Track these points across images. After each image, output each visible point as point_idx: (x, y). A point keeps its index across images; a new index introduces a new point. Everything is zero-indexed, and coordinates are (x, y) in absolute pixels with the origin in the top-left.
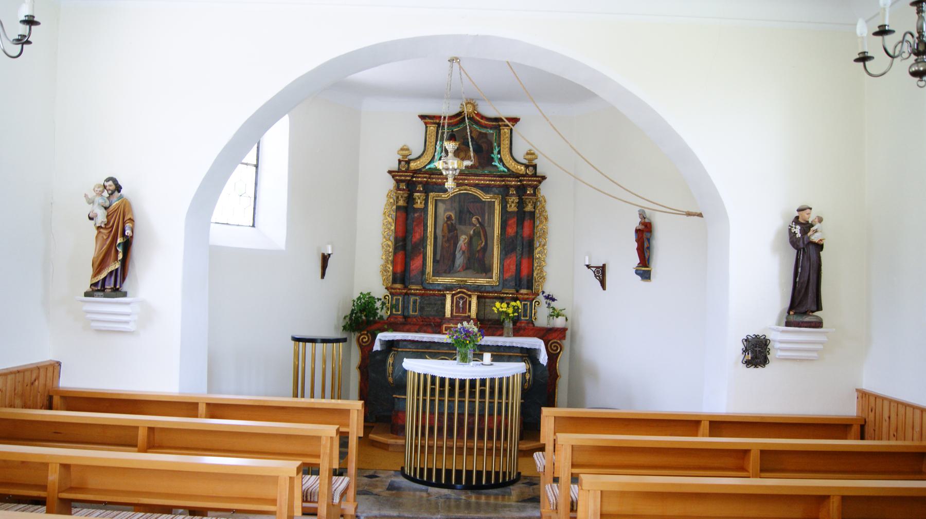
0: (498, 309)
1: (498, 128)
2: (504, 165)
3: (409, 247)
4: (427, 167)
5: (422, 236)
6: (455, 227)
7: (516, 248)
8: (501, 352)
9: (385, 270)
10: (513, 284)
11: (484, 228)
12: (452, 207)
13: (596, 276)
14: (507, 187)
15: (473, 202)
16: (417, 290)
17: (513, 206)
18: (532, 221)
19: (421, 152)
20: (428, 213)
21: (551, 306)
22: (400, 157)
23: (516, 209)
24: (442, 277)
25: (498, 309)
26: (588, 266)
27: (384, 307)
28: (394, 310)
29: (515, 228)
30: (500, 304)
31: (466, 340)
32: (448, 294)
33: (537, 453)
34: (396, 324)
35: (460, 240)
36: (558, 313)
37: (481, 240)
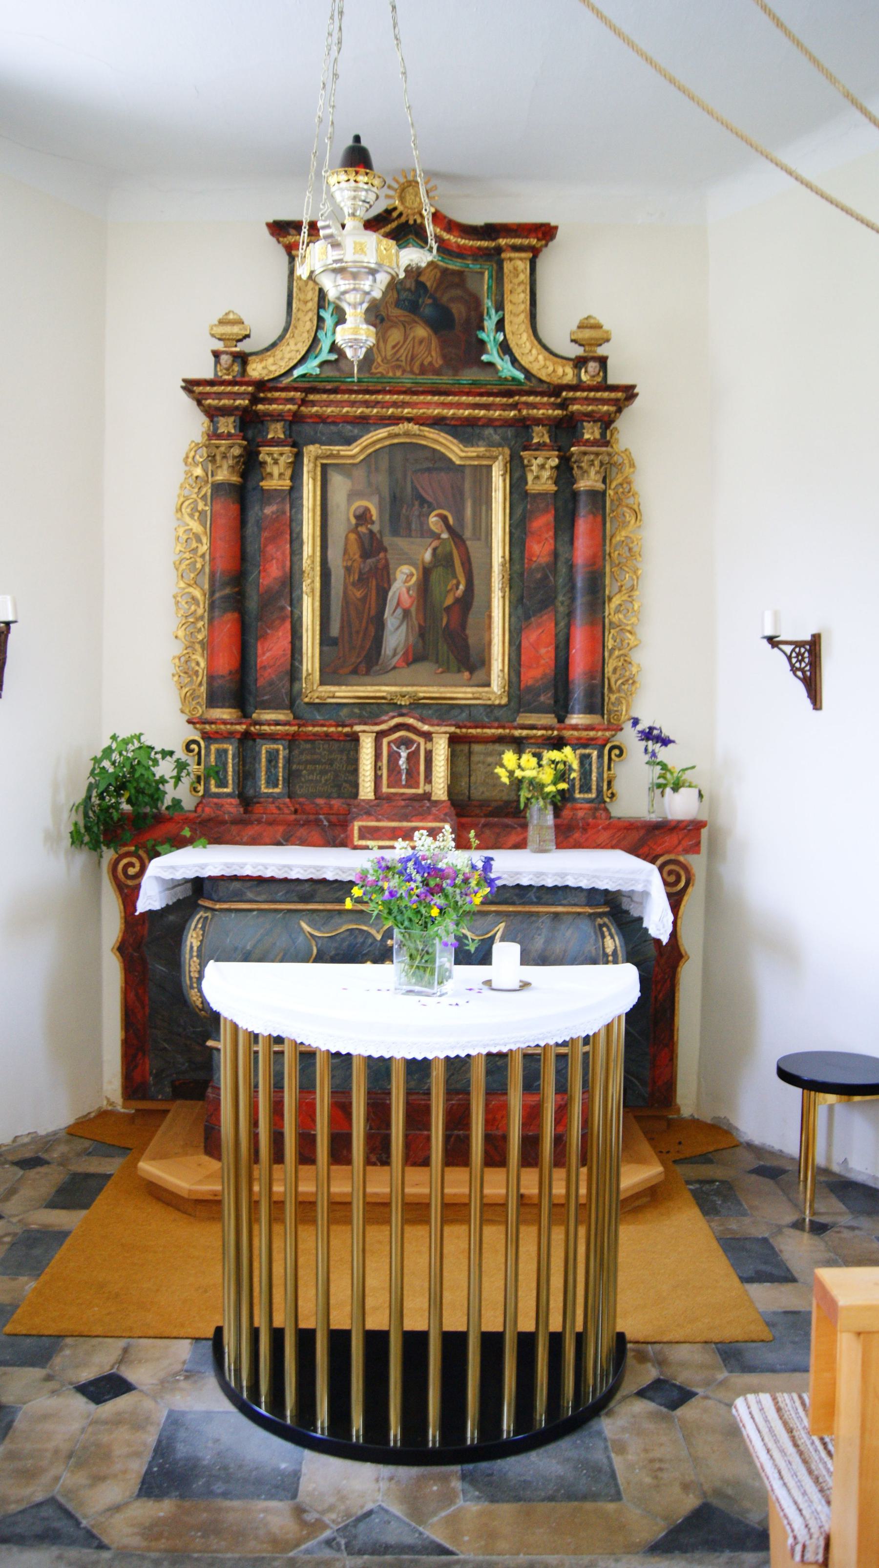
0: (511, 773)
1: (494, 256)
2: (514, 361)
3: (252, 604)
4: (297, 373)
5: (287, 569)
6: (380, 542)
7: (556, 598)
8: (532, 903)
9: (186, 670)
10: (546, 698)
11: (463, 542)
12: (370, 484)
13: (794, 669)
14: (524, 426)
15: (429, 470)
16: (277, 723)
17: (543, 480)
18: (599, 519)
19: (282, 325)
20: (302, 506)
21: (658, 760)
22: (219, 346)
23: (551, 487)
24: (346, 685)
25: (511, 773)
26: (773, 641)
27: (184, 774)
28: (213, 782)
29: (552, 541)
30: (516, 757)
31: (428, 906)
32: (364, 732)
33: (751, 1397)
34: (217, 822)
35: (395, 579)
36: (678, 778)
37: (455, 576)
